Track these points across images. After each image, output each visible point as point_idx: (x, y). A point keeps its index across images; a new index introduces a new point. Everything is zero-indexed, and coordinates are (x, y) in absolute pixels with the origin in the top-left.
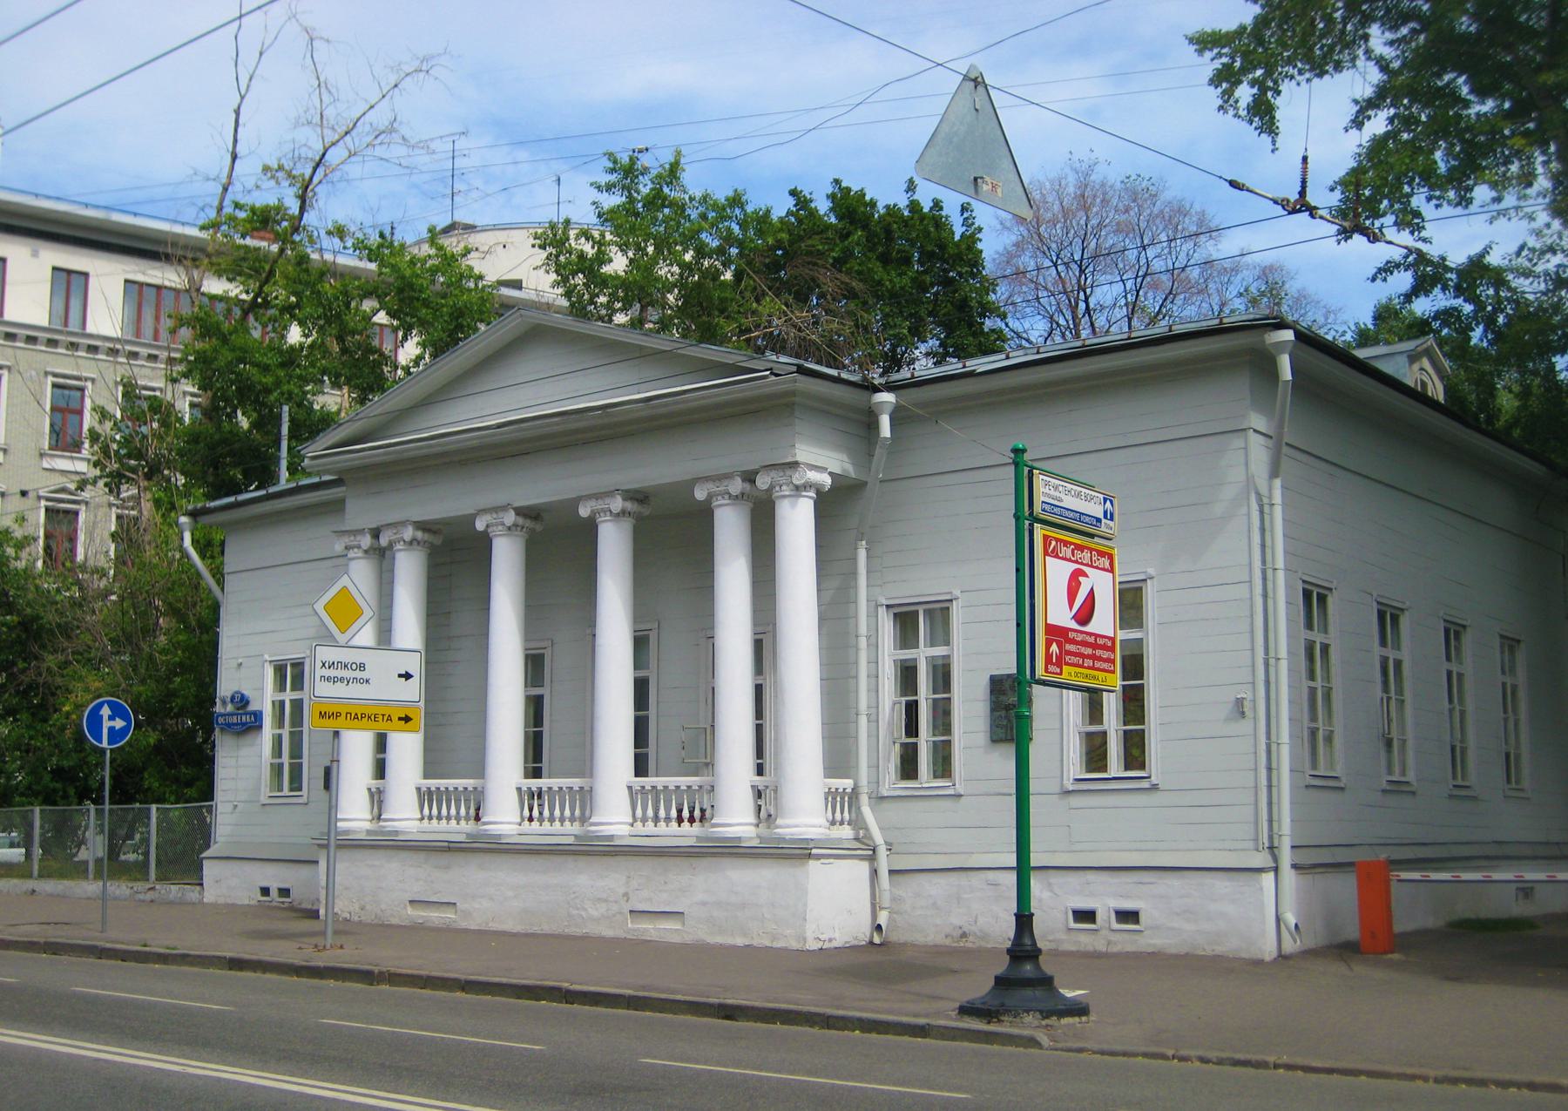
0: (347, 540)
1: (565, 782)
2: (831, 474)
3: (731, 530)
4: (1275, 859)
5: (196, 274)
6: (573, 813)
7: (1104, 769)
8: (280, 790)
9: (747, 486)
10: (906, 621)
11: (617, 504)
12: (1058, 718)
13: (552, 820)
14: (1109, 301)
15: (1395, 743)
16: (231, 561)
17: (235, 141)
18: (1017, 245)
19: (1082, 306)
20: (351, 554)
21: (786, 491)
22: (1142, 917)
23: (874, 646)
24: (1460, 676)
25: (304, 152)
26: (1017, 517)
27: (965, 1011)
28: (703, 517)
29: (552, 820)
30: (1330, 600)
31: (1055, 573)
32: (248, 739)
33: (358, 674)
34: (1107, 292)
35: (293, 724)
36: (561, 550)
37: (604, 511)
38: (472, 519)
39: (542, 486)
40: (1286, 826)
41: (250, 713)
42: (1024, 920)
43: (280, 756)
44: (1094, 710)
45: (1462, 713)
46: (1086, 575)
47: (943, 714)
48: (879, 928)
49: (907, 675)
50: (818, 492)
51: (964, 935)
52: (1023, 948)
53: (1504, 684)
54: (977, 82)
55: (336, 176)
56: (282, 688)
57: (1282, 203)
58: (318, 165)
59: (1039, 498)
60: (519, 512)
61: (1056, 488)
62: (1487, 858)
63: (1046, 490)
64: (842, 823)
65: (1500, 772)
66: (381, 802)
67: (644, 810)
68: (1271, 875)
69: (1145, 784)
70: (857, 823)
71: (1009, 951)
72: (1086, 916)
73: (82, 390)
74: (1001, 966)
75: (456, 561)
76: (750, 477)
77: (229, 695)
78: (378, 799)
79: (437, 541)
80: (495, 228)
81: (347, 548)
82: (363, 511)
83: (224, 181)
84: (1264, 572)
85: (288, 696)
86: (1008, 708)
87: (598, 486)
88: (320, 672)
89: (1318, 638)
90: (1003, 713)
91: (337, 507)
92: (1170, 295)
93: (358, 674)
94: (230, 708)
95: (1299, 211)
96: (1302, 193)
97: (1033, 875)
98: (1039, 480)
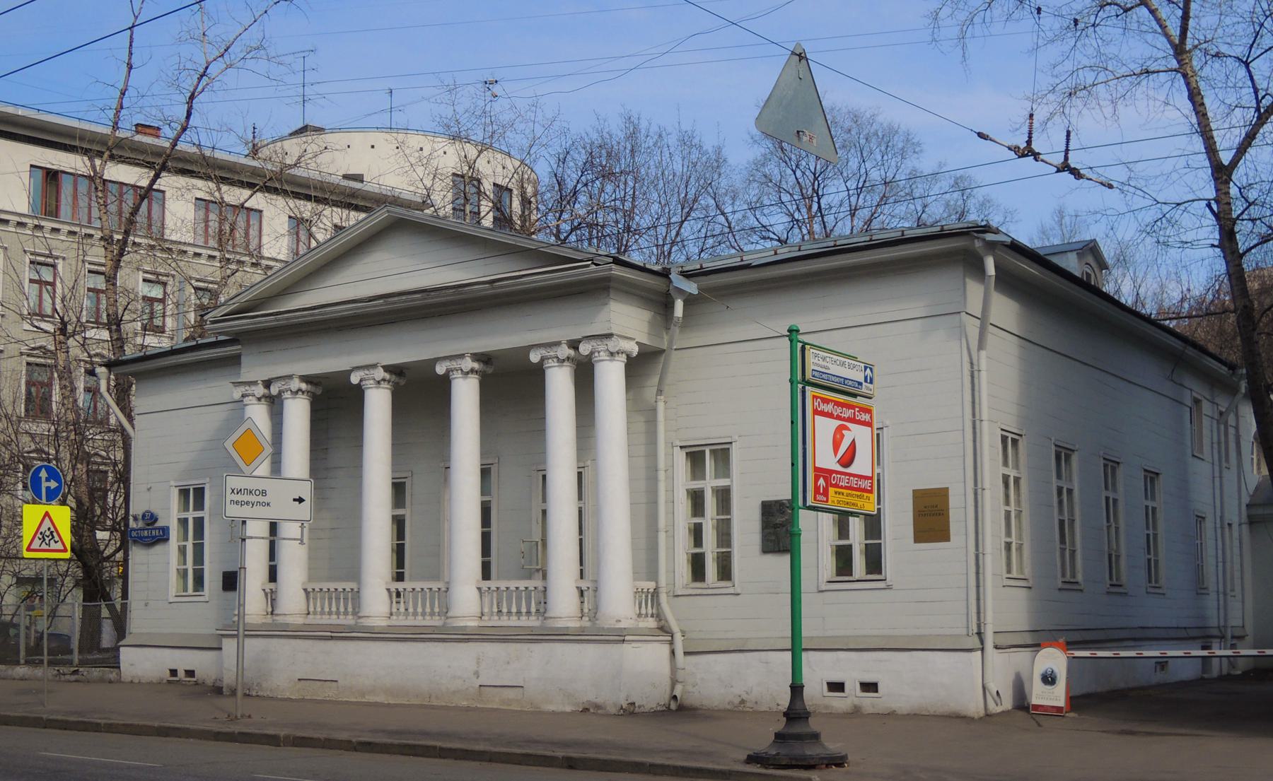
0: (242, 390)
1: (418, 586)
2: (637, 343)
3: (560, 384)
4: (982, 642)
5: (98, 162)
6: (432, 609)
8: (185, 589)
9: (572, 352)
10: (695, 458)
11: (468, 364)
12: (817, 533)
13: (415, 614)
14: (836, 202)
15: (1014, 547)
16: (140, 401)
17: (131, 54)
18: (764, 155)
19: (815, 207)
20: (246, 400)
21: (603, 355)
22: (847, 687)
23: (671, 479)
24: (1115, 501)
25: (189, 65)
26: (791, 381)
27: (751, 759)
28: (537, 375)
29: (415, 614)
30: (1020, 443)
31: (824, 428)
32: (158, 549)
33: (261, 499)
34: (835, 193)
35: (195, 538)
36: (421, 396)
38: (347, 374)
39: (408, 349)
40: (989, 617)
41: (159, 529)
42: (797, 689)
43: (185, 564)
44: (843, 531)
45: (1117, 529)
46: (848, 429)
47: (724, 536)
48: (675, 697)
49: (697, 499)
50: (628, 357)
51: (743, 702)
52: (796, 712)
53: (1147, 507)
54: (801, 57)
55: (216, 85)
56: (186, 509)
57: (1015, 149)
58: (202, 76)
59: (810, 367)
60: (387, 368)
61: (824, 359)
62: (1134, 639)
63: (815, 361)
64: (646, 615)
65: (1143, 573)
66: (273, 600)
67: (424, 606)
68: (979, 653)
69: (881, 585)
70: (658, 616)
71: (785, 714)
72: (837, 687)
73: (54, 266)
74: (780, 725)
75: (335, 405)
76: (574, 345)
77: (140, 513)
78: (272, 598)
79: (319, 391)
80: (340, 130)
81: (243, 396)
82: (256, 368)
83: (121, 86)
84: (974, 423)
85: (191, 515)
86: (776, 526)
87: (456, 351)
88: (230, 497)
89: (1013, 474)
90: (772, 530)
91: (235, 361)
92: (884, 200)
93: (261, 499)
94: (141, 524)
95: (1027, 155)
96: (1029, 142)
97: (804, 654)
98: (810, 353)
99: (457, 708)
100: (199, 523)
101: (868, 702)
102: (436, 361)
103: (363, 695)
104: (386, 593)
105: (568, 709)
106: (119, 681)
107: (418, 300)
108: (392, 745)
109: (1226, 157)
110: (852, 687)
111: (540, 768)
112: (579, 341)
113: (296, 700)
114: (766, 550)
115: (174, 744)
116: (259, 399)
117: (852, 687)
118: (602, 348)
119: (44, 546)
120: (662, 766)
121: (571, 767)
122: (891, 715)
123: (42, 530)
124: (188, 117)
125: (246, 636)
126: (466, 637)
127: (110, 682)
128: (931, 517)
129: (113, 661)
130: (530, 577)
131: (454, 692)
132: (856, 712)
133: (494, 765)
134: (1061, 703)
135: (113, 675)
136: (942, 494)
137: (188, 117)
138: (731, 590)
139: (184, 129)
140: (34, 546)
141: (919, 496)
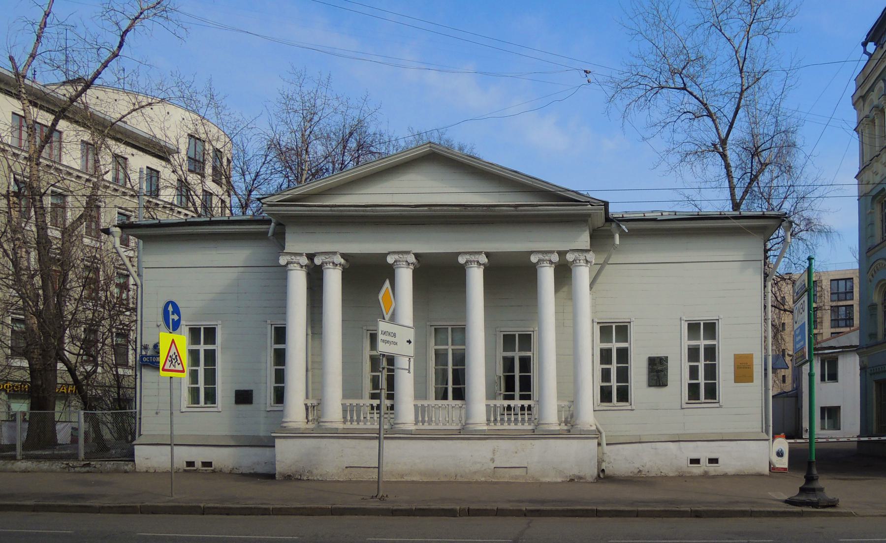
3: (547, 275)
7: (699, 399)
11: (484, 259)
22: (701, 462)
36: (439, 279)
37: (546, 260)
43: (609, 380)
48: (603, 471)
51: (640, 471)
69: (717, 405)
82: (299, 244)
85: (202, 348)
86: (658, 371)
87: (474, 249)
99: (477, 482)
100: (211, 357)
101: (712, 469)
102: (459, 254)
103: (402, 476)
104: (304, 407)
105: (559, 480)
106: (134, 472)
107: (457, 211)
108: (557, 510)
109: (738, 198)
110: (704, 461)
111: (484, 518)
112: (566, 252)
113: (342, 482)
114: (650, 385)
115: (347, 519)
116: (302, 267)
117: (704, 461)
118: (582, 257)
119: (172, 368)
120: (760, 512)
121: (697, 517)
122: (725, 475)
123: (171, 354)
124: (120, 46)
125: (386, 438)
126: (484, 436)
127: (126, 472)
128: (657, 372)
129: (130, 456)
130: (495, 399)
131: (475, 473)
132: (705, 475)
133: (335, 517)
134: (786, 466)
135: (129, 467)
136: (750, 357)
137: (120, 46)
138: (629, 408)
139: (115, 55)
140: (167, 367)
141: (737, 357)
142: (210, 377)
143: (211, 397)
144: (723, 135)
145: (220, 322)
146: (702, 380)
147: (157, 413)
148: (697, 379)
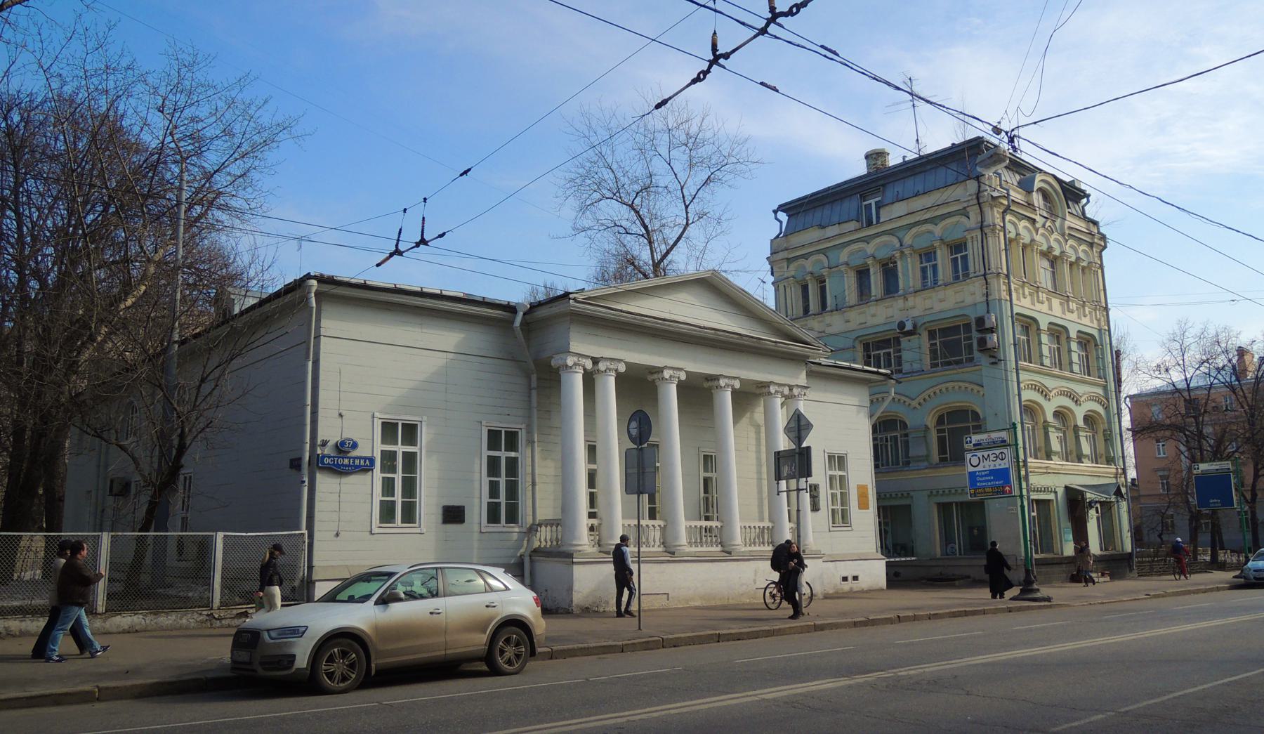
69: (418, 530)
100: (410, 460)
138: (418, 530)
142: (410, 487)
143: (409, 514)
144: (658, 257)
145: (425, 418)
146: (398, 498)
147: (337, 535)
148: (393, 495)
